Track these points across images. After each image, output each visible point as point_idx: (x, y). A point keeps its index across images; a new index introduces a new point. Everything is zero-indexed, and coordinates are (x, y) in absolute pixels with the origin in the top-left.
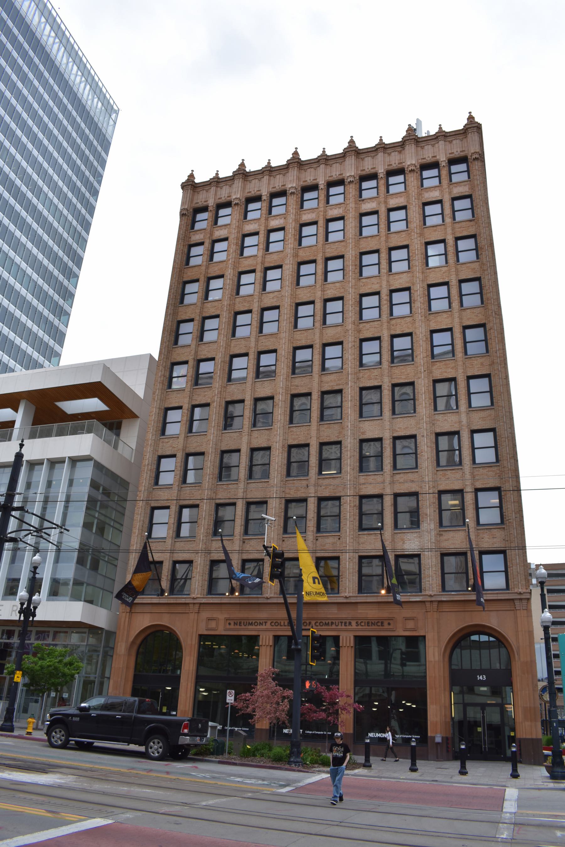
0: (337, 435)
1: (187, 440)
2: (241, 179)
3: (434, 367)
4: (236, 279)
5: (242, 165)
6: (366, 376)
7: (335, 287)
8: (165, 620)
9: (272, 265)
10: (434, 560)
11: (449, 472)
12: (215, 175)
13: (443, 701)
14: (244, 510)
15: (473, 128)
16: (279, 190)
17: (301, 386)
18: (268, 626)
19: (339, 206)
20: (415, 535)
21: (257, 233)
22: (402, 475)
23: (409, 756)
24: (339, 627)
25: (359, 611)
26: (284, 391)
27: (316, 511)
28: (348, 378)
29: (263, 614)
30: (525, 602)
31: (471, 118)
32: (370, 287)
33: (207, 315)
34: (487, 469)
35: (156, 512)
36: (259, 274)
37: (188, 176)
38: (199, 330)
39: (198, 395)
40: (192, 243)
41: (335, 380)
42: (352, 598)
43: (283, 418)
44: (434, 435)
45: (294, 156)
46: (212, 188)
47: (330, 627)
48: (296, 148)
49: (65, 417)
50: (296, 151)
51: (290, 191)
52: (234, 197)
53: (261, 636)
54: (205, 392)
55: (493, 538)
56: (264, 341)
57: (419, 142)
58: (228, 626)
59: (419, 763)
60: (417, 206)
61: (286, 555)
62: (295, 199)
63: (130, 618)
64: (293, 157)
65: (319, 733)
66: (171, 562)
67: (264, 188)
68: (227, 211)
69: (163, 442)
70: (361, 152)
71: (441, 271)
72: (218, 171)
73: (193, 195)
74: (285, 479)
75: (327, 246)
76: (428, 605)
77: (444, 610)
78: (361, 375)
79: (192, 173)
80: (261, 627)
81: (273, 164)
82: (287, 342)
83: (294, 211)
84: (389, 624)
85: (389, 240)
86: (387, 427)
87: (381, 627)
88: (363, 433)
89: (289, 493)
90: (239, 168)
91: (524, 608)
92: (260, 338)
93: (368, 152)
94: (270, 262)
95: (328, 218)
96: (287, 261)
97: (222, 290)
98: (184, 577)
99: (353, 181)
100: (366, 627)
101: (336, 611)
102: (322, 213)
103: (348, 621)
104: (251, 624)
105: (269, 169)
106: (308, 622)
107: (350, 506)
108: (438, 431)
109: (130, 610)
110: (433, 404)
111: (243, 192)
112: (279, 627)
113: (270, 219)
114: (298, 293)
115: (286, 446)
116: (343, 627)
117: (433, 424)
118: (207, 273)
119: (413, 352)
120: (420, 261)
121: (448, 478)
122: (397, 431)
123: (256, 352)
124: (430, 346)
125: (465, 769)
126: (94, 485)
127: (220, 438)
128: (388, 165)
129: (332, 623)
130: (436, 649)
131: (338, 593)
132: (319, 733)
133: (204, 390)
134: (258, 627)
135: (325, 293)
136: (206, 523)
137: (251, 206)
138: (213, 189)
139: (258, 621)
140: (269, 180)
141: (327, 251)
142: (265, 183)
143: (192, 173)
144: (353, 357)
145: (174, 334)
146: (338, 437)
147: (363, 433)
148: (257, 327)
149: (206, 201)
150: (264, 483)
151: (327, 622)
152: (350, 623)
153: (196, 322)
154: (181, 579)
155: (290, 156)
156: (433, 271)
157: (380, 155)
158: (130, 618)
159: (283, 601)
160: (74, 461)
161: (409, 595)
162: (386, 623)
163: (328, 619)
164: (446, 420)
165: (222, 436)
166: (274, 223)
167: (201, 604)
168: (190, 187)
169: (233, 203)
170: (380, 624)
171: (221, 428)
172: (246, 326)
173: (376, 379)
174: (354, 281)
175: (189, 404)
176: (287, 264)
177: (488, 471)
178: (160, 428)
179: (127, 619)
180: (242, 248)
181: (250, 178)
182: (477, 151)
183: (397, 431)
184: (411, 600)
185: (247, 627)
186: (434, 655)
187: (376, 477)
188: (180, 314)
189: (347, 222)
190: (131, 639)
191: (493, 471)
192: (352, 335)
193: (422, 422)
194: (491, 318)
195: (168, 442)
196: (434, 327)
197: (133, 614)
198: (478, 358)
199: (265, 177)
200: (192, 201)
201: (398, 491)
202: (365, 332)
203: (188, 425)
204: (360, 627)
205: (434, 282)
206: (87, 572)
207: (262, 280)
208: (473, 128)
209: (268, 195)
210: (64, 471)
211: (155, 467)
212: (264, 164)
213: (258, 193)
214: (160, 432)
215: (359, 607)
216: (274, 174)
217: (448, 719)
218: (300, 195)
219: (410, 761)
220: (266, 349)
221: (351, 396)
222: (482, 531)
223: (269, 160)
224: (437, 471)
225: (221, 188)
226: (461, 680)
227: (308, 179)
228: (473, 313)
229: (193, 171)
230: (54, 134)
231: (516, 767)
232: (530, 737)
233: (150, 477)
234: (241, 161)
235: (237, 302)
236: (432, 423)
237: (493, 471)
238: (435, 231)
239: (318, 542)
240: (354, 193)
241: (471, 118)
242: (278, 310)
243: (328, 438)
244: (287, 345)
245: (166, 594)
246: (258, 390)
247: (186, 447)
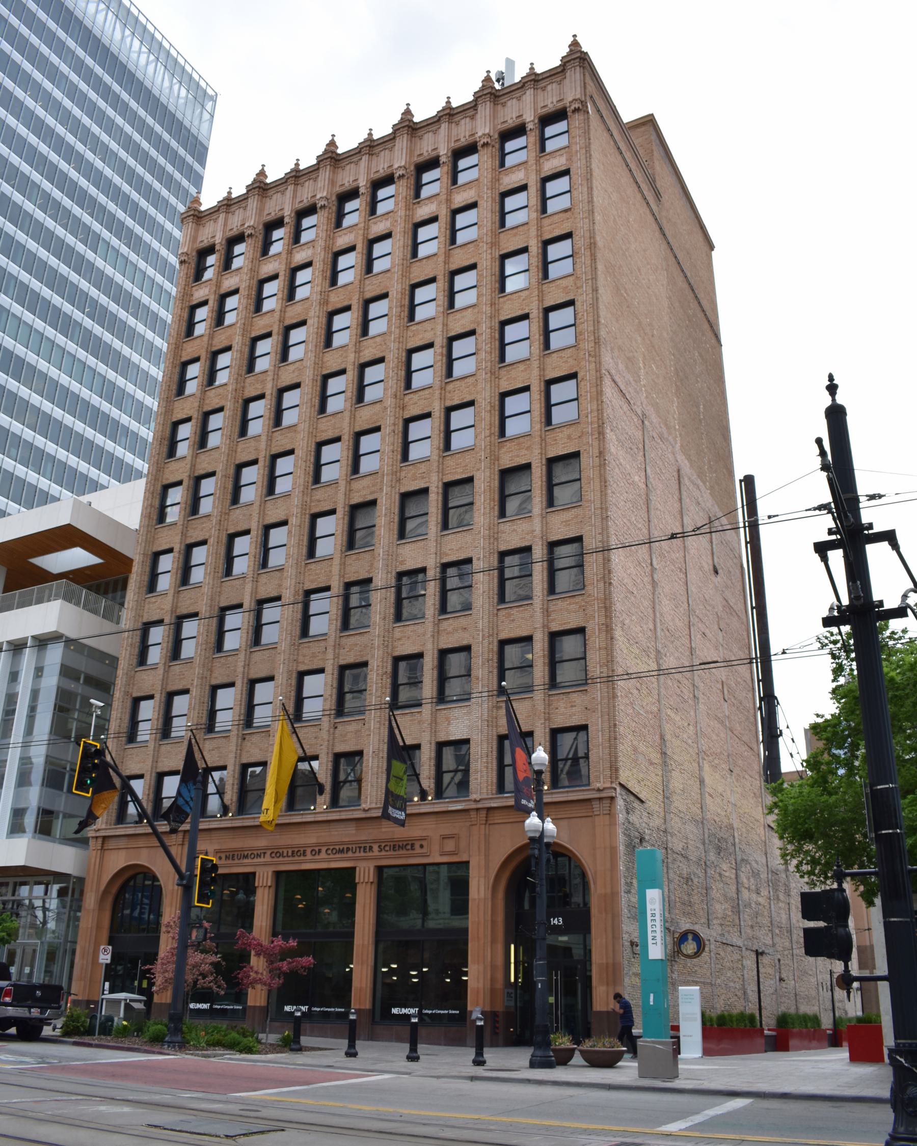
0: (367, 568)
1: (178, 597)
2: (405, 136)
3: (503, 450)
4: (247, 350)
5: (408, 113)
6: (410, 475)
9: (295, 321)
10: (485, 746)
11: (514, 611)
12: (293, 166)
13: (489, 959)
14: (244, 692)
15: (577, 59)
16: (513, 125)
17: (325, 500)
18: (268, 858)
19: (386, 217)
20: (465, 710)
21: (523, 188)
22: (451, 621)
23: (347, 1036)
24: (357, 854)
25: (383, 830)
26: (299, 510)
27: (335, 685)
28: (382, 482)
29: (260, 842)
30: (606, 803)
31: (575, 44)
32: (421, 336)
33: (210, 409)
34: (568, 601)
35: (307, 679)
36: (442, 283)
37: (327, 145)
38: (198, 432)
40: (194, 303)
41: (368, 487)
42: (373, 811)
43: (296, 552)
44: (496, 556)
45: (572, 48)
46: (364, 158)
47: (345, 855)
48: (575, 36)
49: (44, 577)
50: (575, 40)
51: (573, 108)
52: (480, 134)
53: (357, 869)
54: (203, 523)
55: (572, 706)
56: (280, 438)
57: (499, 96)
59: (422, 1048)
60: (490, 199)
61: (504, 730)
62: (326, 215)
63: (102, 858)
64: (571, 50)
65: (442, 1012)
66: (154, 775)
67: (440, 144)
68: (472, 160)
69: (149, 603)
70: (419, 126)
71: (520, 297)
72: (371, 130)
73: (197, 231)
74: (297, 641)
75: (546, 222)
76: (473, 814)
77: (496, 821)
78: (403, 474)
79: (333, 140)
80: (259, 860)
81: (539, 70)
82: (306, 435)
83: (324, 235)
84: (422, 846)
85: (451, 259)
86: (433, 550)
87: (411, 852)
88: (402, 563)
89: (303, 663)
90: (483, 86)
92: (275, 434)
93: (428, 125)
94: (292, 318)
95: (371, 237)
96: (312, 314)
97: (475, 289)
98: (570, 756)
99: (403, 176)
100: (392, 853)
101: (354, 832)
102: (361, 232)
103: (368, 845)
104: (246, 857)
105: (533, 77)
106: (317, 849)
107: (378, 674)
108: (503, 548)
109: (102, 847)
110: (496, 508)
111: (410, 157)
112: (281, 859)
113: (294, 251)
114: (325, 359)
115: (301, 592)
116: (362, 854)
117: (497, 539)
118: (210, 344)
120: (489, 286)
121: (513, 620)
122: (447, 555)
123: (268, 457)
124: (497, 418)
125: (354, 1048)
126: (66, 671)
127: (218, 590)
128: (455, 141)
129: (348, 849)
130: (482, 881)
131: (589, 785)
132: (442, 1012)
134: (255, 860)
135: (362, 354)
136: (196, 715)
137: (510, 146)
138: (444, 126)
139: (255, 852)
140: (295, 191)
141: (366, 289)
142: (528, 101)
143: (333, 140)
144: (391, 447)
145: (166, 443)
146: (368, 572)
147: (402, 563)
148: (269, 419)
149: (521, 116)
151: (341, 847)
152: (371, 848)
153: (227, 412)
154: (566, 760)
155: (565, 50)
156: (508, 300)
157: (529, 95)
158: (102, 858)
160: (42, 642)
162: (417, 846)
163: (343, 843)
164: (514, 530)
165: (221, 586)
166: (551, 165)
167: (489, 809)
168: (577, 63)
169: (480, 144)
170: (409, 847)
171: (220, 575)
172: (521, 341)
173: (423, 478)
174: (397, 330)
175: (181, 543)
176: (311, 318)
177: (570, 604)
178: (145, 583)
179: (98, 860)
180: (503, 215)
181: (270, 193)
182: (578, 96)
183: (447, 555)
184: (450, 809)
185: (241, 861)
186: (480, 889)
187: (416, 627)
188: (175, 412)
189: (574, 177)
190: (103, 887)
191: (577, 603)
192: (392, 414)
193: (477, 540)
194: (583, 363)
196: (505, 386)
197: (106, 852)
198: (565, 429)
199: (528, 92)
200: (194, 238)
201: (445, 646)
202: (411, 408)
203: (179, 575)
204: (383, 853)
205: (509, 317)
206: (64, 797)
207: (280, 346)
208: (577, 59)
209: (536, 121)
210: (28, 657)
211: (138, 640)
212: (362, 137)
213: (434, 154)
214: (145, 589)
216: (457, 118)
217: (500, 985)
218: (497, 146)
219: (408, 1045)
221: (386, 509)
222: (556, 698)
223: (532, 64)
224: (498, 610)
225: (457, 124)
226: (519, 926)
227: (508, 118)
228: (561, 357)
229: (333, 136)
230: (117, 125)
231: (482, 1050)
232: (605, 1009)
233: (130, 654)
234: (261, 168)
235: (247, 384)
236: (494, 537)
237: (577, 603)
238: (515, 235)
239: (337, 731)
240: (404, 194)
241: (575, 44)
242: (572, 308)
243: (356, 575)
244: (305, 441)
245: (430, 798)
246: (269, 513)
247: (177, 607)
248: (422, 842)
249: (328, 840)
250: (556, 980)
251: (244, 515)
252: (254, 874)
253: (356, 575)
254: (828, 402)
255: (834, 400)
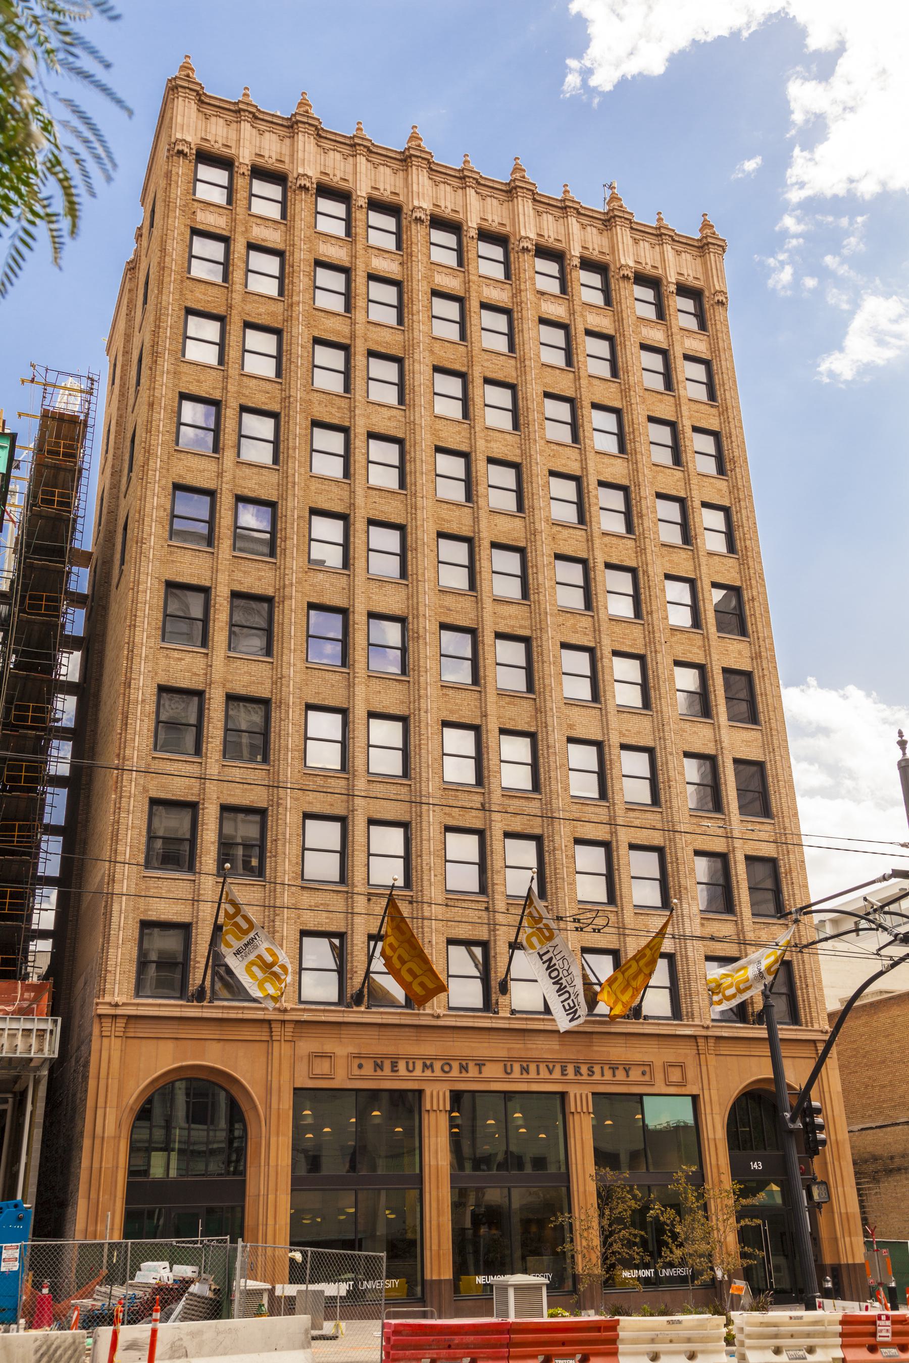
7: (505, 440)
8: (213, 1056)
39: (245, 572)
53: (428, 1093)
54: (259, 570)
58: (356, 1071)
77: (722, 1053)
91: (117, 1034)
101: (557, 1047)
119: (211, 530)
133: (256, 565)
150: (399, 787)
159: (766, 1036)
161: (676, 1025)
184: (678, 1033)
195: (181, 659)
215: (594, 1040)
220: (383, 518)
248: (648, 1074)
249: (523, 1054)
250: (17, 589)
251: (332, 585)
252: (420, 1092)
253: (513, 723)
254: (899, 755)
255: (904, 754)
